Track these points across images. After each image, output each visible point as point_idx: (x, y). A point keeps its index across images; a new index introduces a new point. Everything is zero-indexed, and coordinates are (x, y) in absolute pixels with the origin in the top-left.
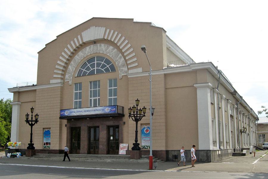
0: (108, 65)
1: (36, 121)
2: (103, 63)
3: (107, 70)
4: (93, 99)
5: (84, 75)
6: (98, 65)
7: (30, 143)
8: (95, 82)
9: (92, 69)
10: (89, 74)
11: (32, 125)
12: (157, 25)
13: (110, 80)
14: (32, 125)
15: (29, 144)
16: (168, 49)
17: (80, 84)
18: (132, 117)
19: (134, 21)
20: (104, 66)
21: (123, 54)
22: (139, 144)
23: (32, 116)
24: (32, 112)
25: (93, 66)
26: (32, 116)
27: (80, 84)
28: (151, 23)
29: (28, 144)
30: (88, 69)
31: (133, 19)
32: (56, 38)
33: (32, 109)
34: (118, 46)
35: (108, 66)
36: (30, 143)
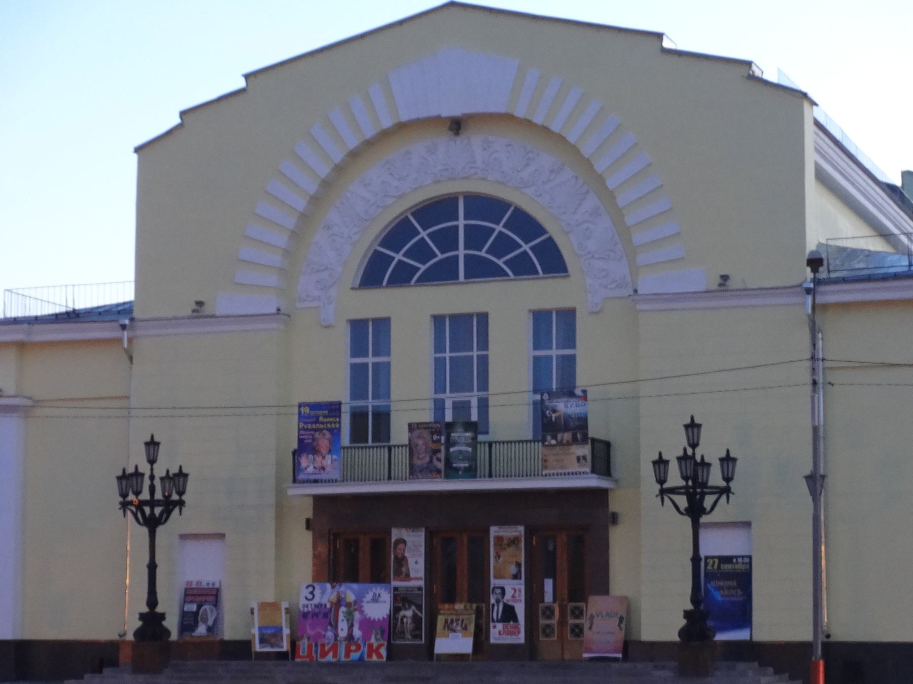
0: (498, 223)
1: (170, 505)
2: (526, 247)
3: (523, 267)
4: (370, 360)
5: (402, 277)
6: (476, 237)
7: (145, 609)
8: (460, 321)
9: (440, 256)
10: (429, 278)
11: (152, 524)
12: (770, 76)
13: (540, 318)
14: (152, 524)
15: (142, 616)
16: (822, 177)
17: (382, 325)
18: (676, 498)
19: (666, 44)
20: (503, 246)
21: (608, 196)
22: (162, 616)
23: (152, 477)
24: (152, 461)
25: (447, 240)
26: (152, 477)
27: (382, 325)
28: (749, 64)
29: (138, 616)
30: (421, 252)
31: (659, 36)
32: (241, 83)
33: (152, 445)
34: (606, 188)
35: (526, 247)
36: (145, 609)
